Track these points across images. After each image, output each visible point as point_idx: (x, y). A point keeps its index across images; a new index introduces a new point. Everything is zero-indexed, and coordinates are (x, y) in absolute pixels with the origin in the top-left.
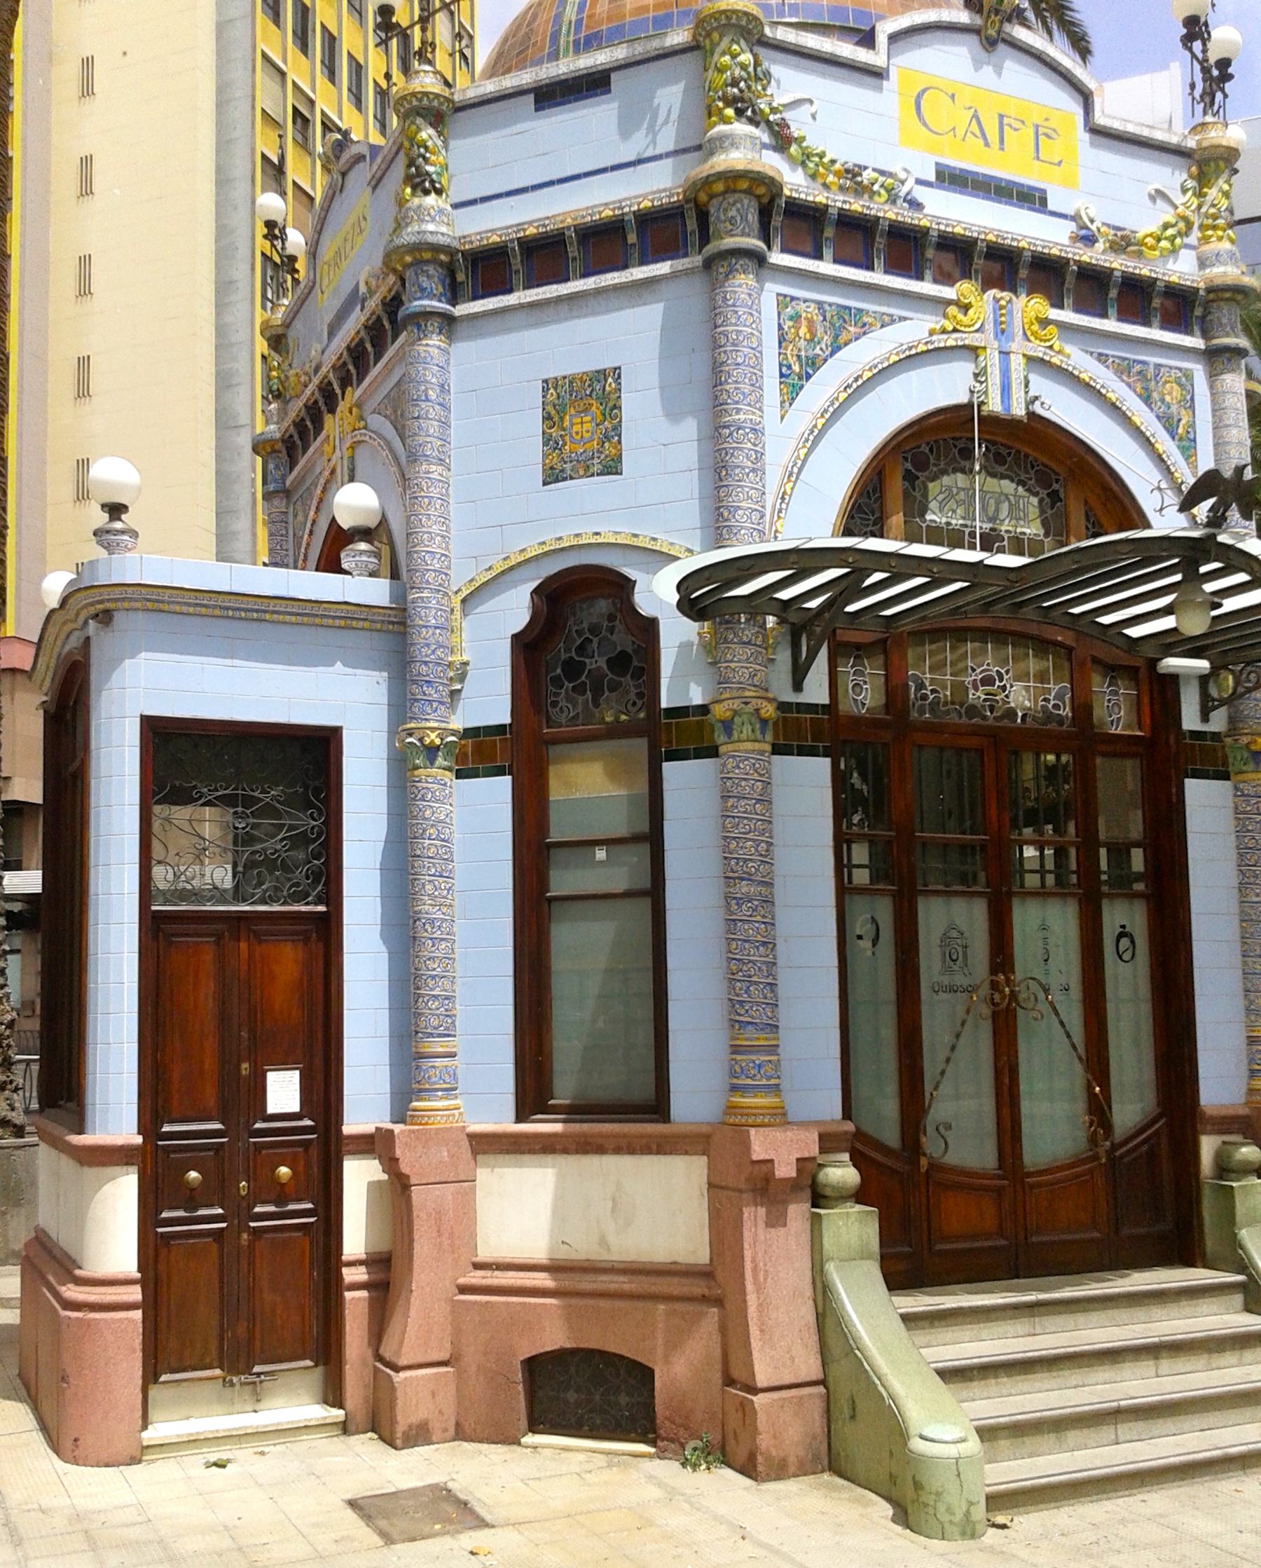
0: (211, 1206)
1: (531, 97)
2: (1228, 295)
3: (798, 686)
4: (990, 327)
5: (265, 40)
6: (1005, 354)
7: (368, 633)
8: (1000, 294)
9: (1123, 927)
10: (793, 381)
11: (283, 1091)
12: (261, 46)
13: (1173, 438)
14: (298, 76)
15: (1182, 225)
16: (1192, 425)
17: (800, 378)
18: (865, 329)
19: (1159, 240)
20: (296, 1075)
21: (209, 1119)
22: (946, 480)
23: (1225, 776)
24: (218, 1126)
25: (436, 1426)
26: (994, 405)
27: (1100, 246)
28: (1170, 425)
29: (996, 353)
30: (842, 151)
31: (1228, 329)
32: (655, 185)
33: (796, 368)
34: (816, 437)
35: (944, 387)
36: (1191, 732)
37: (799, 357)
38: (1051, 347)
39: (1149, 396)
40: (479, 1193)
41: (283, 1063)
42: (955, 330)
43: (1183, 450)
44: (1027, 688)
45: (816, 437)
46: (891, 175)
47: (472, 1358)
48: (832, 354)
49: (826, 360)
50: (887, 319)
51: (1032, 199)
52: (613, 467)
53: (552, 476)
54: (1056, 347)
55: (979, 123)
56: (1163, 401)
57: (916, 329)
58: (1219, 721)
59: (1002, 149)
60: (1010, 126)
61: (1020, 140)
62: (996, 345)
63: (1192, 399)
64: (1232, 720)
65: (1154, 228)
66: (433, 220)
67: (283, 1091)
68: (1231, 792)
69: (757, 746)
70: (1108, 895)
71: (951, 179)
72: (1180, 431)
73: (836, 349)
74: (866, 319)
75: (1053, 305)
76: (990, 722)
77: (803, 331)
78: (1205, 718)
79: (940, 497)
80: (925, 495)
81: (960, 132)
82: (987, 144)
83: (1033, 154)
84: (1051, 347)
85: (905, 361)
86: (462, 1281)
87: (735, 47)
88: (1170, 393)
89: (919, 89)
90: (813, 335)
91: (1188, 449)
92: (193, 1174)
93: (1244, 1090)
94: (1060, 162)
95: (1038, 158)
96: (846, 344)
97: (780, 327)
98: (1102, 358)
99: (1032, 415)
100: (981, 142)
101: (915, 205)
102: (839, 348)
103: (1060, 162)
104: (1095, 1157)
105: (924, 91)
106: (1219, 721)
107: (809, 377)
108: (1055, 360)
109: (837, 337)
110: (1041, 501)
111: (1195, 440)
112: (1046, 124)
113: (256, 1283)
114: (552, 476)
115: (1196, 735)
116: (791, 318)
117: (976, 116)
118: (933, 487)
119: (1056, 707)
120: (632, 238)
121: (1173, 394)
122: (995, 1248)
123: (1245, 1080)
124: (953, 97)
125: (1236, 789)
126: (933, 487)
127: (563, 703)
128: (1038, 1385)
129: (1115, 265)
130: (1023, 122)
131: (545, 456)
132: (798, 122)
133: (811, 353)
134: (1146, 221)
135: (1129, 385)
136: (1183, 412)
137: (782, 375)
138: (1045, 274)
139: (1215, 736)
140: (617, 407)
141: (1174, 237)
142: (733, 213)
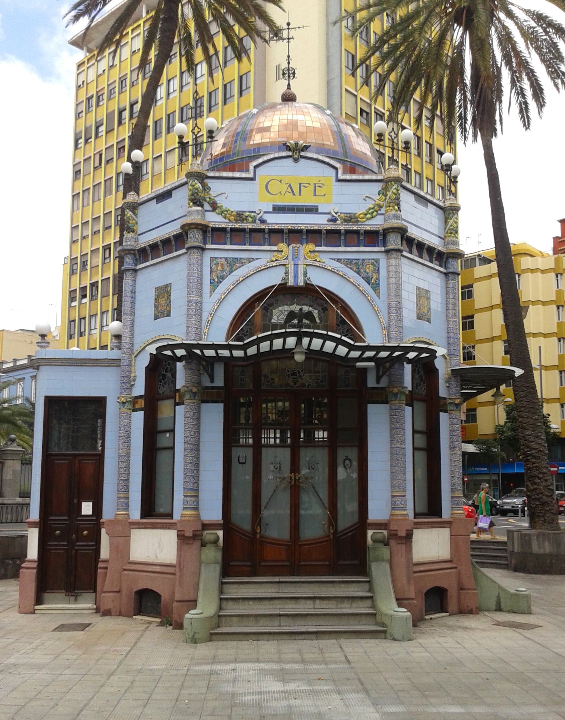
0: (64, 541)
1: (155, 200)
2: (391, 230)
3: (212, 381)
4: (290, 257)
5: (347, 84)
6: (296, 265)
7: (116, 368)
8: (294, 245)
9: (347, 457)
10: (214, 285)
11: (87, 508)
12: (345, 86)
13: (369, 284)
14: (363, 95)
15: (377, 208)
16: (378, 279)
17: (217, 283)
18: (243, 264)
19: (366, 215)
20: (91, 503)
21: (64, 515)
22: (280, 308)
23: (387, 402)
24: (66, 518)
25: (113, 611)
26: (291, 282)
27: (339, 222)
28: (368, 280)
29: (293, 266)
30: (235, 207)
31: (392, 242)
32: (174, 229)
33: (216, 280)
34: (221, 301)
35: (273, 278)
36: (371, 388)
37: (217, 276)
38: (316, 260)
39: (359, 271)
40: (131, 540)
41: (87, 500)
42: (276, 260)
43: (373, 288)
44: (310, 376)
45: (221, 301)
46: (255, 212)
47: (124, 591)
48: (230, 274)
49: (227, 276)
50: (251, 260)
51: (312, 210)
52: (169, 315)
53: (156, 317)
54: (318, 260)
55: (291, 188)
56: (365, 272)
57: (263, 260)
58: (384, 382)
59: (300, 195)
60: (304, 186)
61: (307, 192)
62: (293, 262)
63: (379, 269)
64: (390, 382)
65: (364, 211)
66: (130, 241)
67: (87, 508)
68: (389, 407)
69: (192, 401)
70: (303, 446)
71: (278, 209)
72: (372, 281)
73: (231, 272)
74: (243, 261)
75: (316, 246)
76: (295, 388)
77: (219, 268)
78: (378, 382)
79: (277, 315)
80: (272, 314)
81: (283, 193)
82: (294, 195)
83: (313, 194)
84: (316, 260)
85: (261, 270)
86: (124, 567)
87: (194, 183)
88: (368, 269)
89: (267, 181)
90: (223, 269)
91: (376, 287)
92: (58, 532)
93: (389, 514)
94: (324, 195)
95: (315, 195)
96: (235, 270)
97: (211, 268)
98: (339, 260)
99: (306, 284)
100: (292, 194)
101: (263, 221)
102: (233, 272)
103: (324, 195)
104: (329, 536)
105: (269, 181)
106: (384, 382)
107: (221, 282)
108: (317, 264)
109: (232, 268)
110: (318, 312)
111: (379, 284)
112: (320, 182)
113: (69, 565)
114: (156, 317)
115: (373, 388)
116: (215, 264)
117: (290, 186)
118: (275, 311)
119: (322, 381)
120: (173, 243)
121: (370, 269)
122: (284, 565)
123: (390, 511)
124: (281, 181)
125: (390, 407)
126: (275, 311)
127: (162, 388)
128: (264, 607)
129: (342, 228)
130: (309, 184)
131: (155, 311)
132: (220, 201)
133: (222, 275)
134: (359, 209)
135: (350, 268)
136: (374, 274)
137: (211, 283)
138: (313, 235)
139: (382, 388)
140: (170, 296)
141: (373, 212)
142: (191, 235)
